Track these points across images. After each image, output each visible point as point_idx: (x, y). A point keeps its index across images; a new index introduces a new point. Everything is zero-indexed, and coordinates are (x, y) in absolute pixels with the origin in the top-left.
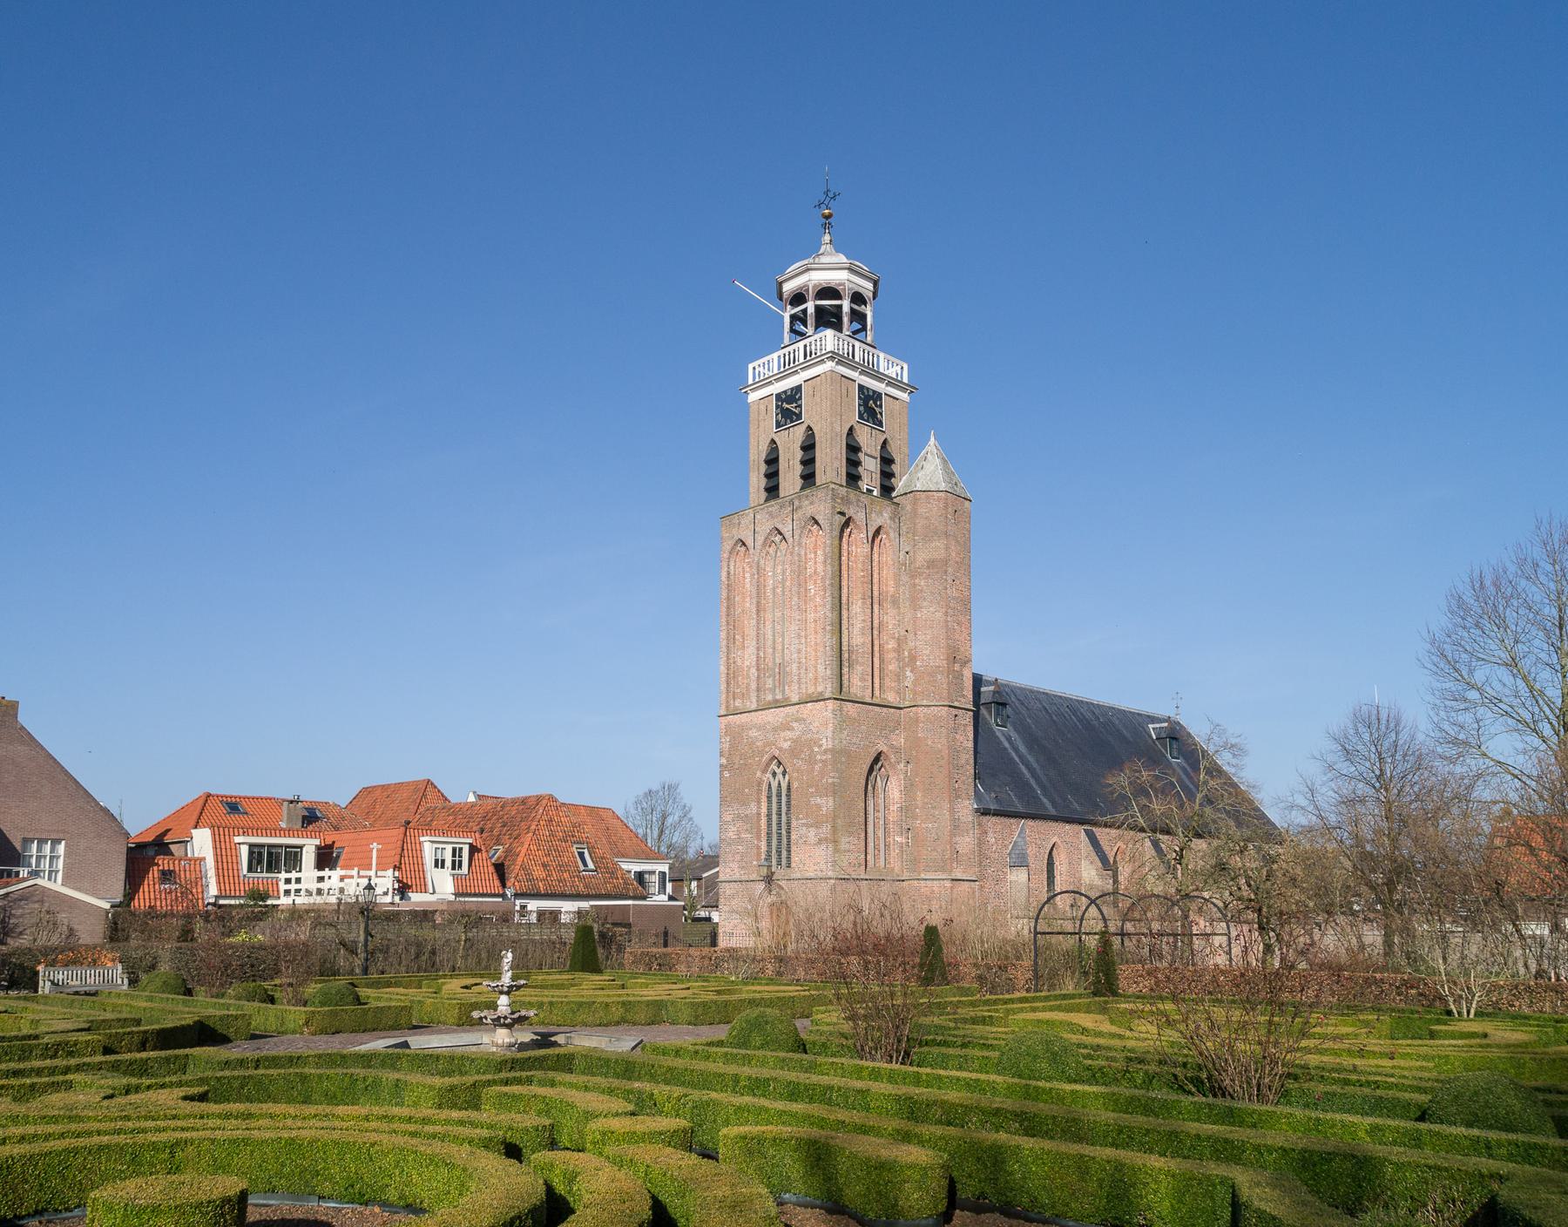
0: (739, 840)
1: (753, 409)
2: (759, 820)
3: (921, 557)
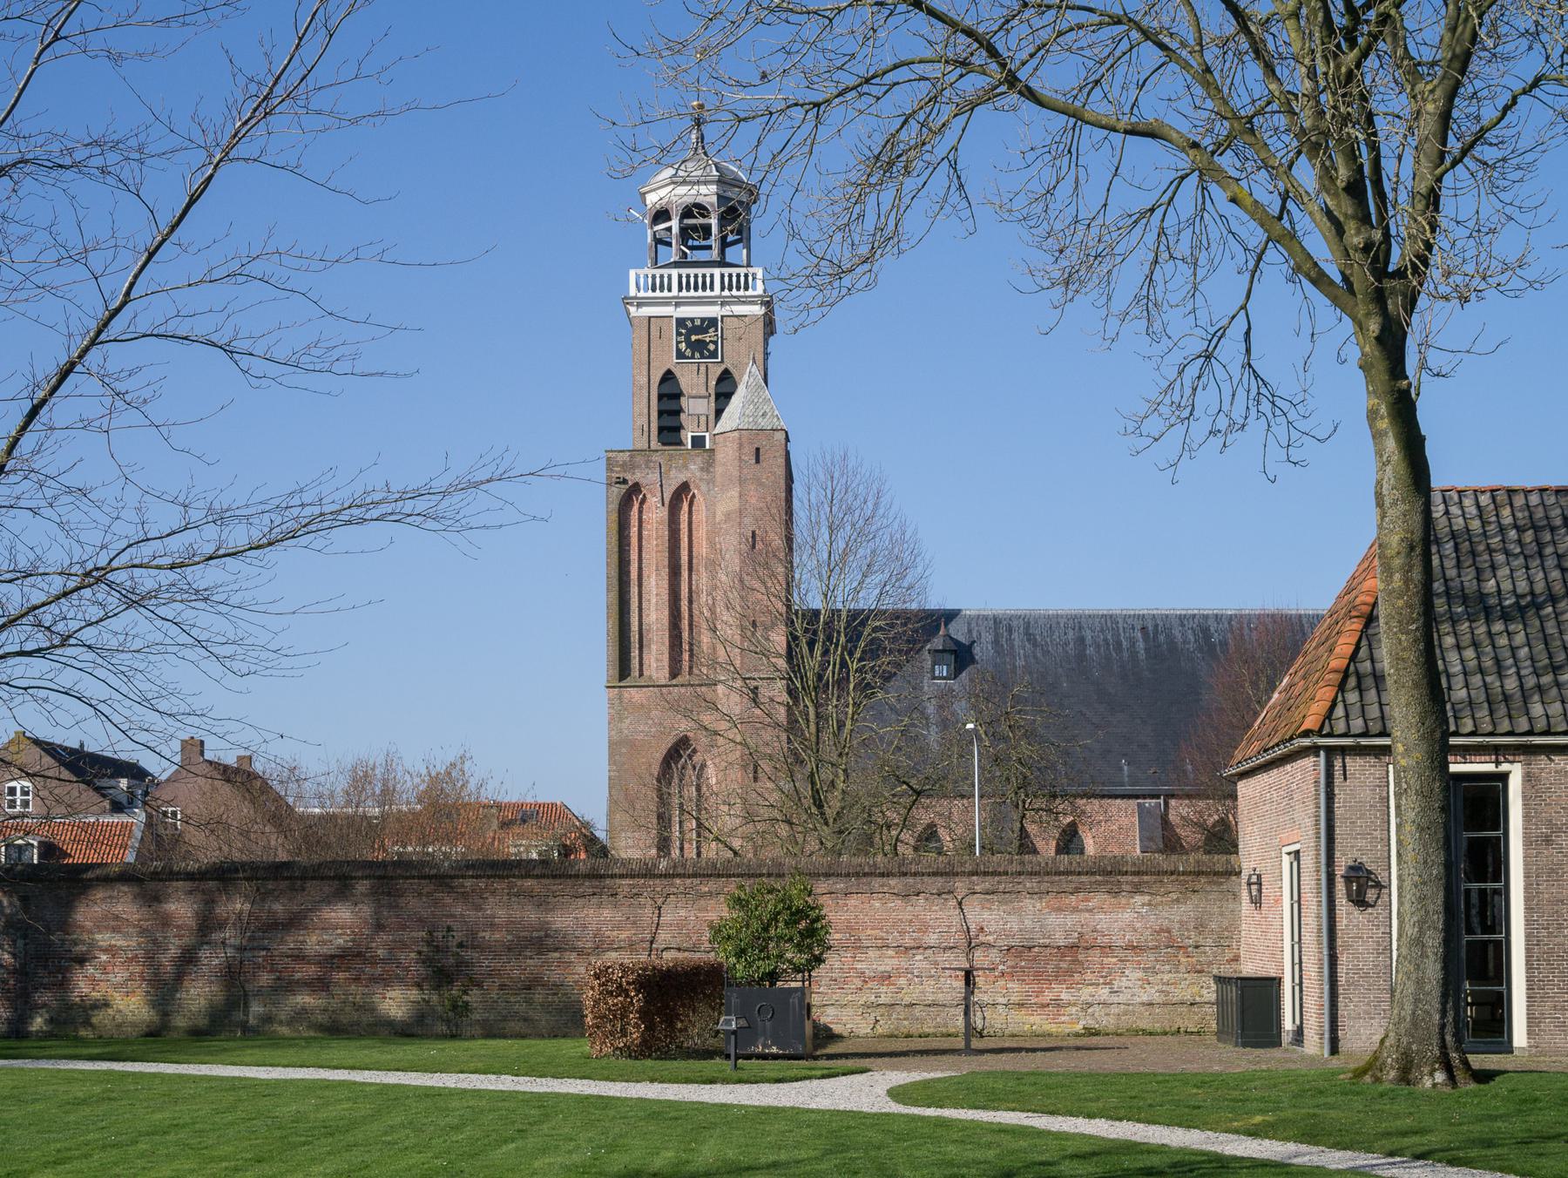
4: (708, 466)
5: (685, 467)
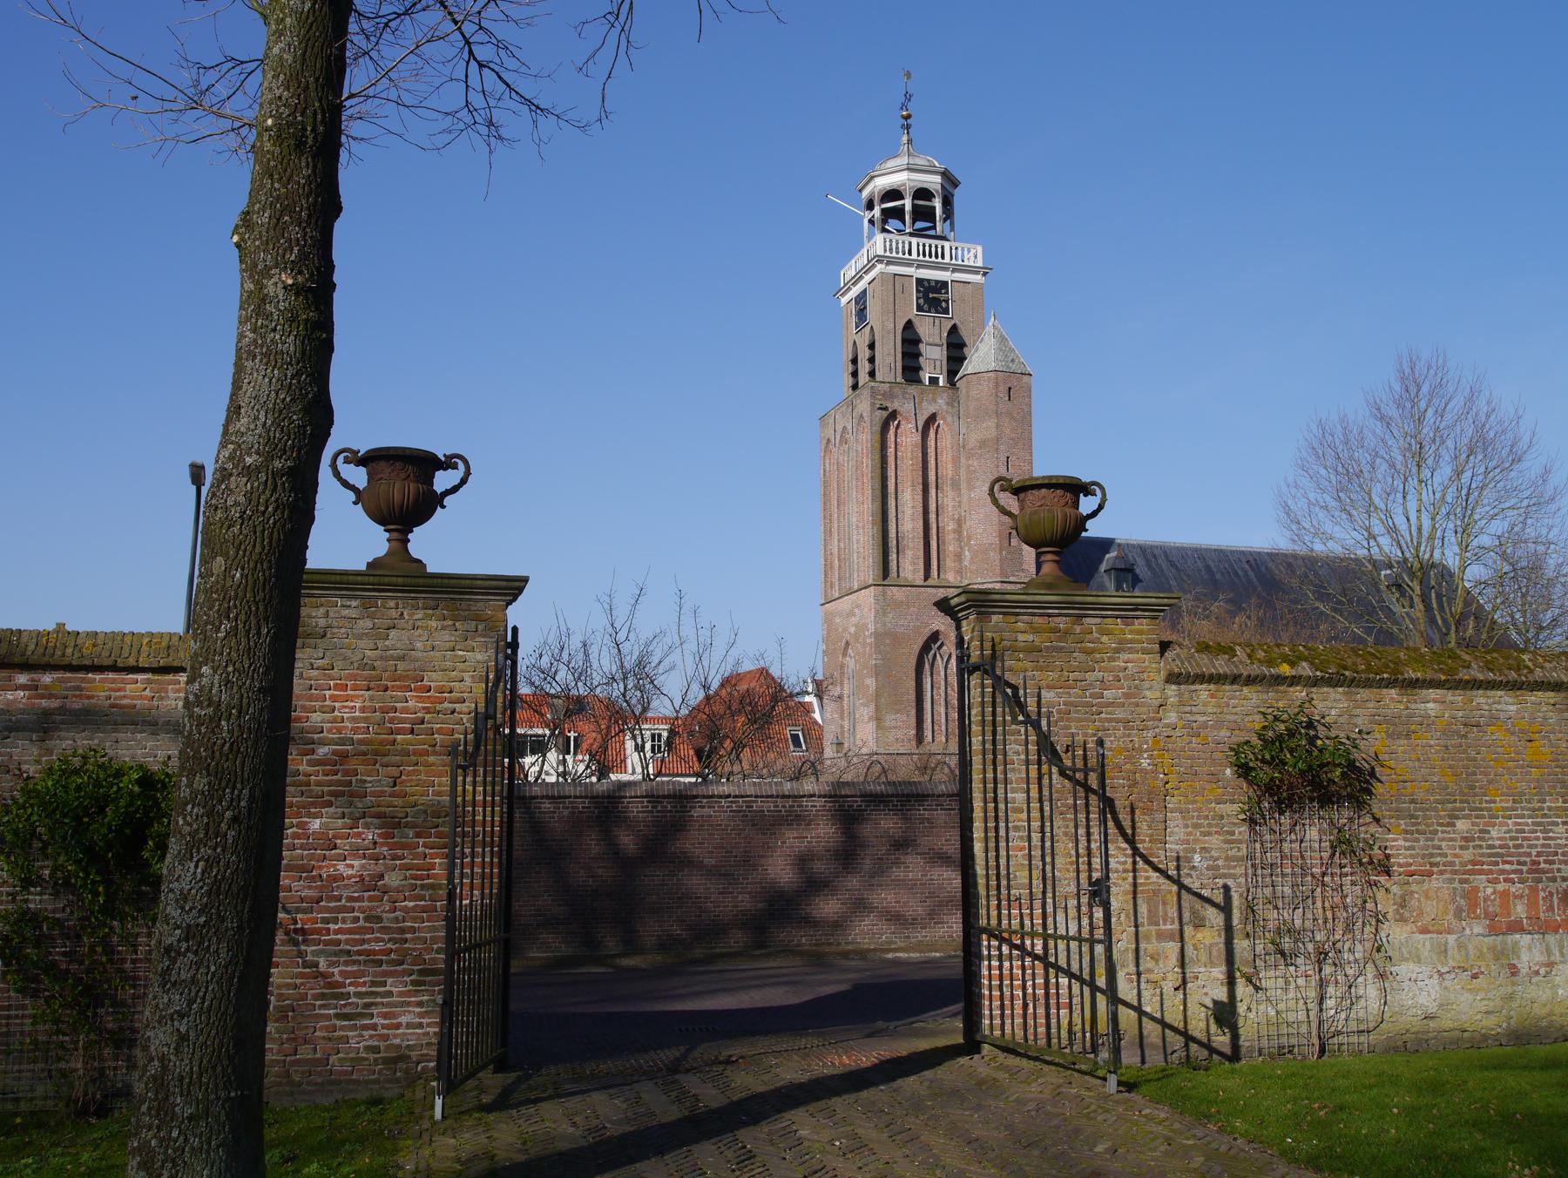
3: (974, 439)
4: (954, 401)
5: (934, 400)
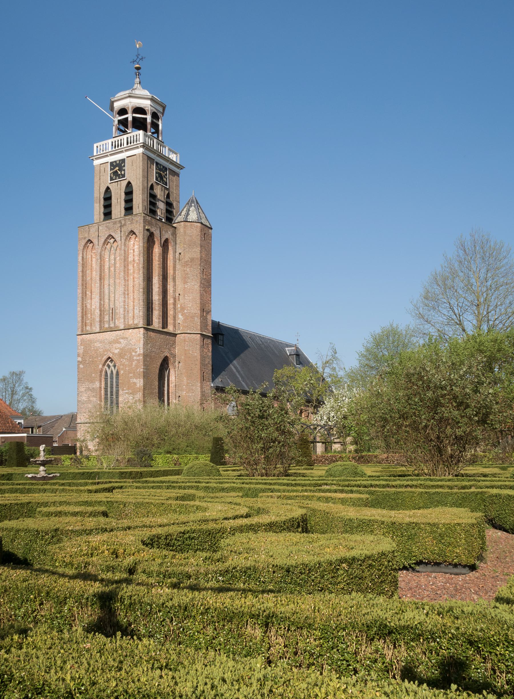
0: (89, 401)
1: (97, 169)
2: (101, 390)
